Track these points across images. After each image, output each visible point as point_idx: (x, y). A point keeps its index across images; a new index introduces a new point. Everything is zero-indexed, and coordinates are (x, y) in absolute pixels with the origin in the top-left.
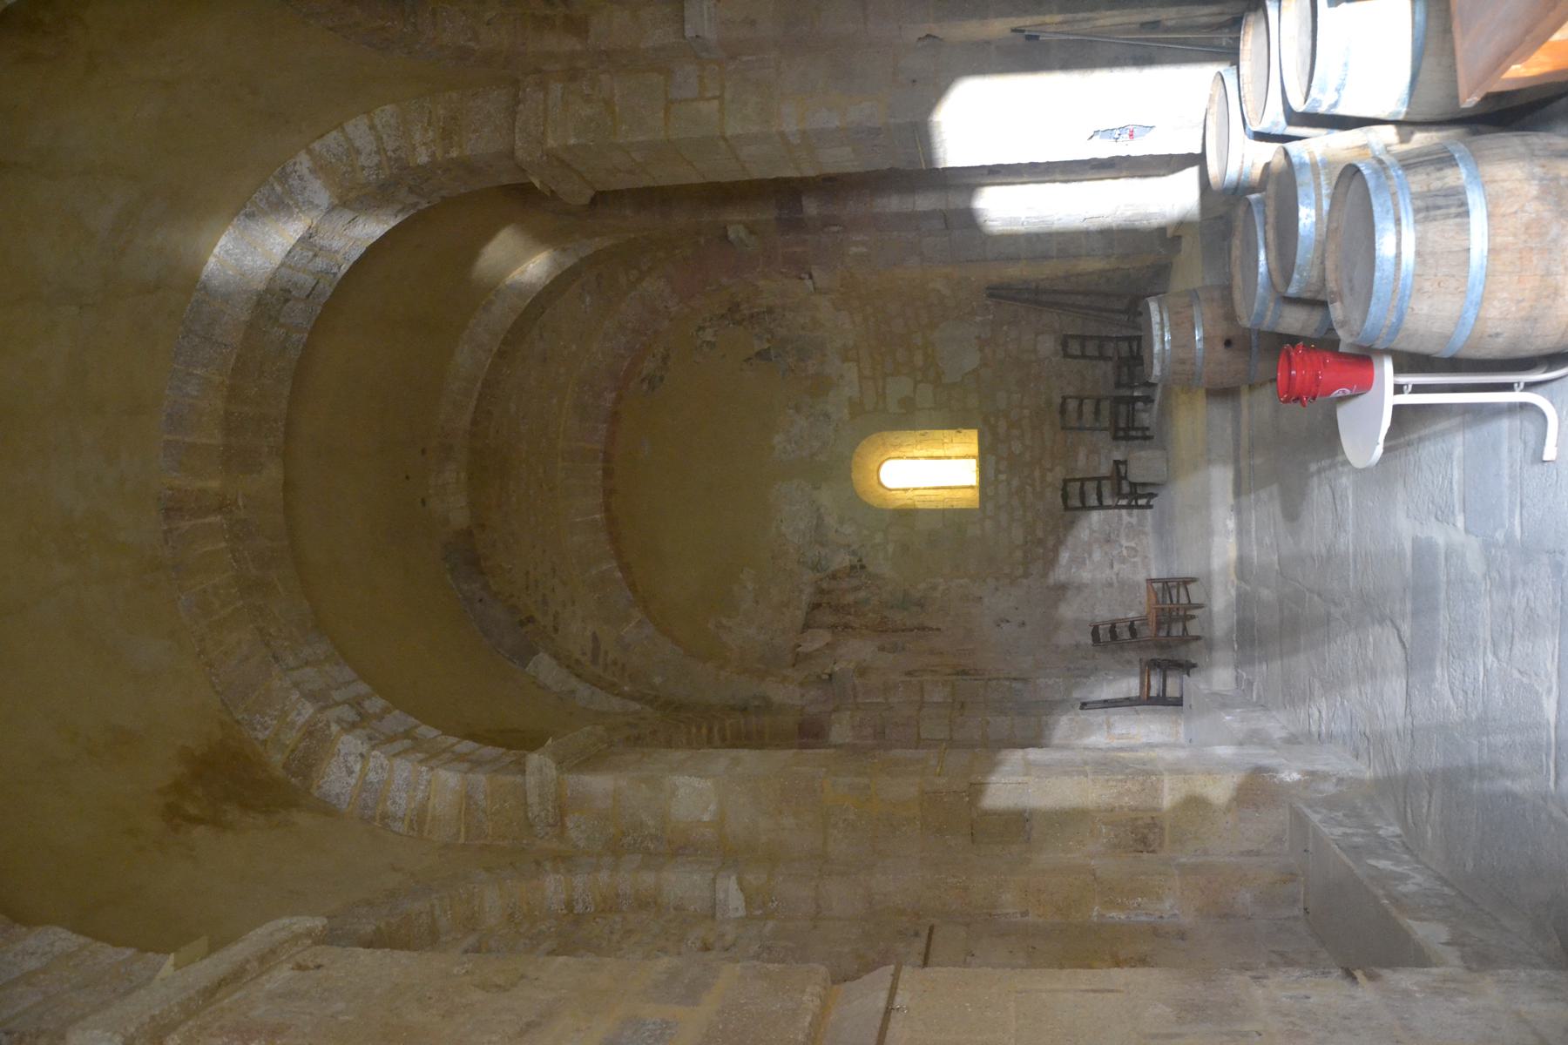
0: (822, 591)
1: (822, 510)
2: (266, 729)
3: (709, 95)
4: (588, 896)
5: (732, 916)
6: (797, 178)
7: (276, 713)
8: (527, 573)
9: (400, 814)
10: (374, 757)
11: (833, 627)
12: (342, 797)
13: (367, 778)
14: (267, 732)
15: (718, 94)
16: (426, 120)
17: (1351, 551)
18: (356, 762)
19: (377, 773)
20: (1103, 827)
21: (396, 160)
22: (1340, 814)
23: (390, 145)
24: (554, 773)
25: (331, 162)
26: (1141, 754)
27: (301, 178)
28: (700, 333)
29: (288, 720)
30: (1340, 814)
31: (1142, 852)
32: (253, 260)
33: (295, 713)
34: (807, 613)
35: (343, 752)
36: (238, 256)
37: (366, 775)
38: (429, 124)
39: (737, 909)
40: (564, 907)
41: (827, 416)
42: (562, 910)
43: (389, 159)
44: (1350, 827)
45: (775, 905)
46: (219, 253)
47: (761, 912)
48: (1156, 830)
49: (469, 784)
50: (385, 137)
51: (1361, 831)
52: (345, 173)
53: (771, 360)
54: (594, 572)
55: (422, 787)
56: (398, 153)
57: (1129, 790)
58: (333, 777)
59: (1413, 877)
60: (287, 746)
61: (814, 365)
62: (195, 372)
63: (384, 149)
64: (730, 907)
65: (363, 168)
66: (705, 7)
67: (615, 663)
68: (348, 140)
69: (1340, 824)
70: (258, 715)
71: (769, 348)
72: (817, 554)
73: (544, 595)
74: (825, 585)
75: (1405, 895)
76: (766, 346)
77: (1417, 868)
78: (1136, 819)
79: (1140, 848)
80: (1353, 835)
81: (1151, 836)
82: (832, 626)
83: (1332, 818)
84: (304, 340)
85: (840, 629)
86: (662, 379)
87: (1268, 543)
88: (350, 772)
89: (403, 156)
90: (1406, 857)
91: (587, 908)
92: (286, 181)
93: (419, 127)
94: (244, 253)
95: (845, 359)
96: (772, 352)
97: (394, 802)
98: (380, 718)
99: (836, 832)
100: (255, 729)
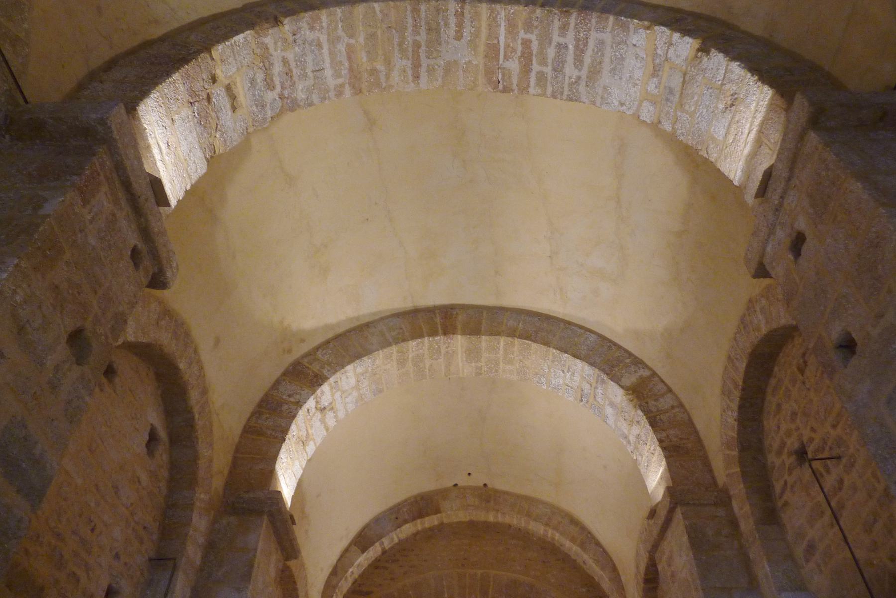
7: (330, 360)
12: (276, 392)
23: (664, 417)
27: (635, 372)
38: (681, 439)
50: (667, 415)
56: (659, 421)
58: (289, 387)
60: (311, 365)
62: (520, 324)
65: (647, 403)
73: (398, 560)
88: (290, 396)
97: (267, 418)
98: (322, 421)
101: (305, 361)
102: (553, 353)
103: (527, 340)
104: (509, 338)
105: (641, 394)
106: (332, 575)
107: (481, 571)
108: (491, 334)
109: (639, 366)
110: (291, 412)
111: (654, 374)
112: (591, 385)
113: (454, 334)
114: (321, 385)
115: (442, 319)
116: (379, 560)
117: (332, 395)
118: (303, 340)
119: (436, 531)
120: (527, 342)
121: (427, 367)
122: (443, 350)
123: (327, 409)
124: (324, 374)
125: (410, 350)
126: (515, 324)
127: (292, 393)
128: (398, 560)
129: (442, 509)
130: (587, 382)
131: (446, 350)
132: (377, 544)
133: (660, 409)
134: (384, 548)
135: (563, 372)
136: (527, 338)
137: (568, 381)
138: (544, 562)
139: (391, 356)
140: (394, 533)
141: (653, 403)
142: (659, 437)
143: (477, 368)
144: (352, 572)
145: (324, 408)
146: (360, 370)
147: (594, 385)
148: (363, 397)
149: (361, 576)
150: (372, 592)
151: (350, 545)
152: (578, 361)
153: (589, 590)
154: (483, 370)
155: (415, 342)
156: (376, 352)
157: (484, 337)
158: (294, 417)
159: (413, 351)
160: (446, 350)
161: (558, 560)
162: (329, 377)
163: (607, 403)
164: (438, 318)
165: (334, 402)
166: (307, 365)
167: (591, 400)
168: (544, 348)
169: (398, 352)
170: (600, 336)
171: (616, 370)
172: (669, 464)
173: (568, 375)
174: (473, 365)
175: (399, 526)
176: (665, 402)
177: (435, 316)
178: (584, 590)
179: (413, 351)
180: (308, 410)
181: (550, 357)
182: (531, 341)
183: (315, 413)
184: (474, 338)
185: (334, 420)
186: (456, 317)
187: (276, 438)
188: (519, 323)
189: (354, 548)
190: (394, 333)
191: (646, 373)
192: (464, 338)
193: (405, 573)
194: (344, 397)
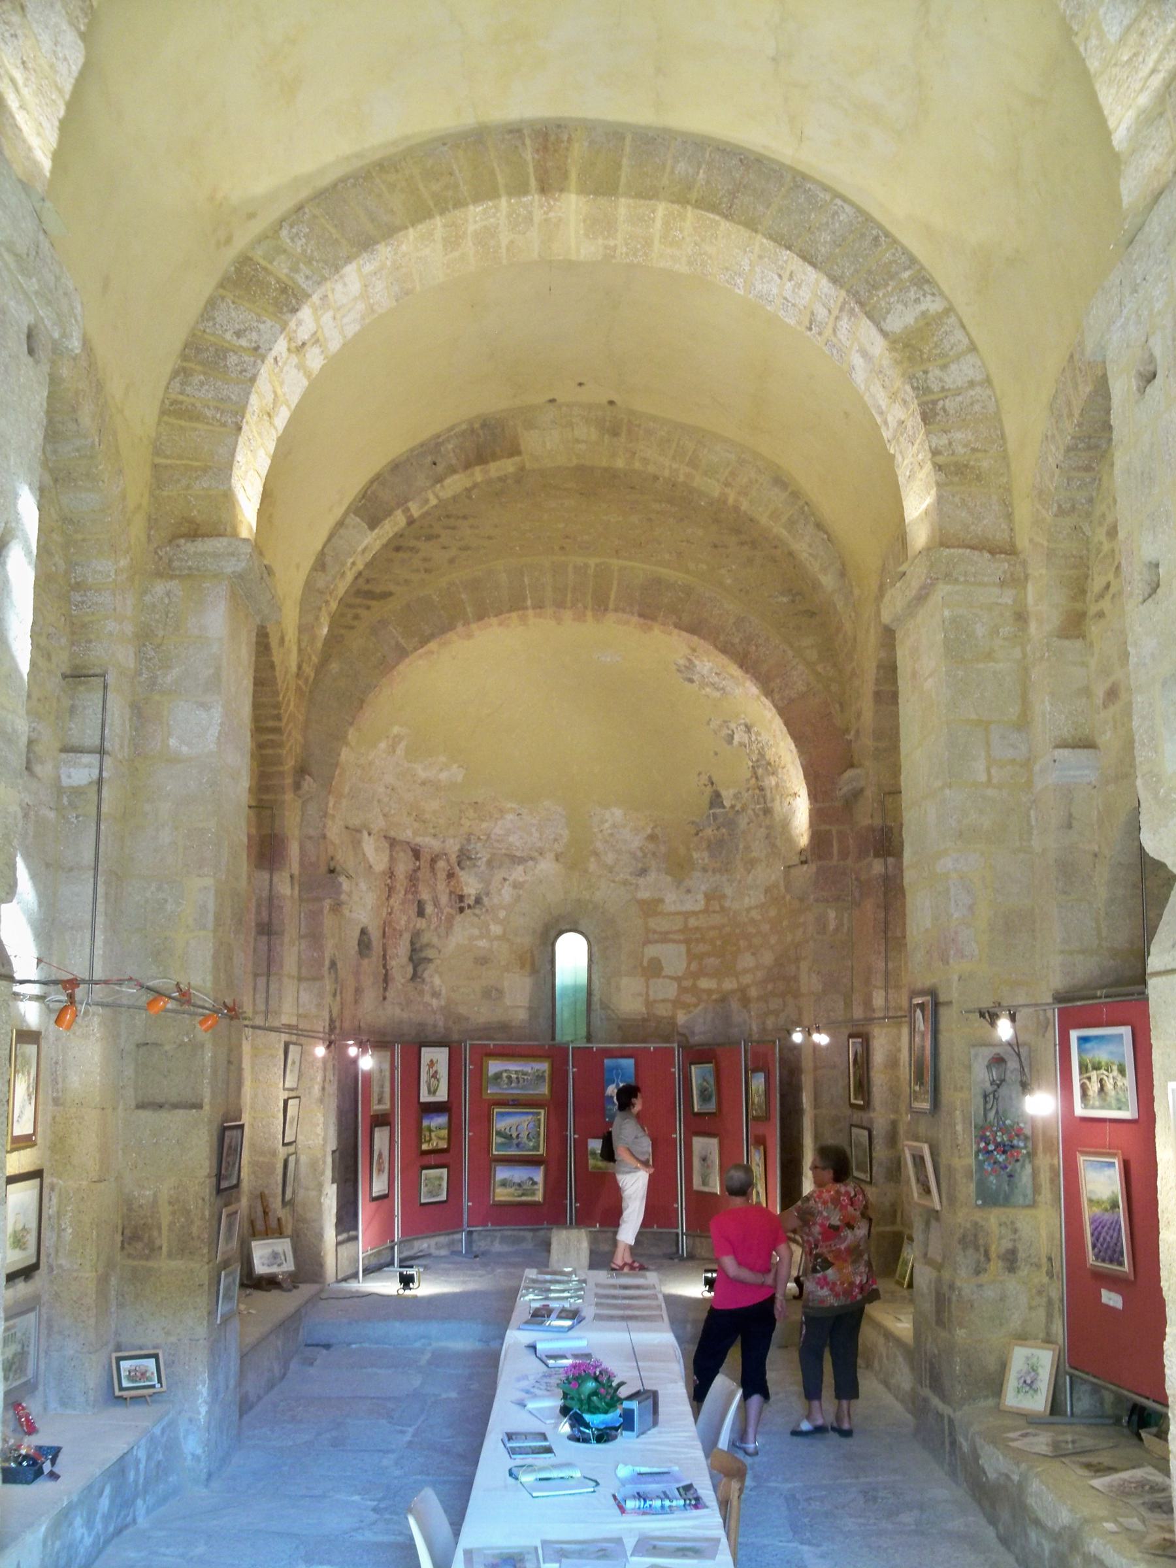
0: (433, 861)
1: (531, 863)
2: (292, 240)
3: (993, 771)
4: (90, 607)
5: (62, 771)
6: (902, 863)
7: (309, 251)
8: (465, 517)
9: (188, 389)
10: (255, 362)
11: (391, 874)
12: (211, 324)
13: (231, 354)
14: (288, 241)
15: (995, 781)
16: (978, 445)
17: (452, 1478)
18: (250, 341)
19: (236, 365)
20: (151, 1192)
21: (932, 410)
22: (160, 1457)
23: (951, 405)
24: (229, 570)
25: (933, 335)
26: (498, 1228)
27: (917, 301)
28: (743, 727)
29: (301, 265)
30: (160, 1457)
31: (123, 1234)
32: (825, 242)
33: (308, 272)
34: (408, 843)
35: (261, 326)
36: (831, 226)
37: (236, 353)
38: (974, 450)
39: (69, 777)
40: (78, 580)
41: (643, 872)
42: (75, 578)
43: (934, 402)
44: (146, 1467)
45: (73, 820)
46: (836, 205)
47: (66, 803)
48: (147, 1252)
49: (220, 470)
50: (959, 399)
51: (141, 1481)
52: (921, 351)
53: (710, 808)
54: (463, 596)
55: (218, 416)
56: (942, 413)
57: (192, 1222)
58: (233, 314)
59: (89, 1535)
60: (271, 262)
61: (703, 859)
62: (701, 171)
63: (946, 397)
64: (72, 770)
65: (926, 372)
66: (1087, 772)
67: (356, 617)
68: (958, 358)
69: (149, 1457)
70: (308, 230)
71: (724, 807)
72: (479, 856)
73: (438, 536)
74: (441, 864)
75: (70, 1525)
76: (727, 803)
77: (99, 1539)
78: (160, 1229)
79: (127, 1232)
80: (137, 1470)
81: (139, 1245)
82: (392, 873)
83: (156, 1448)
84: (737, 291)
85: (389, 881)
86: (691, 681)
87: (472, 1387)
88: (238, 334)
89: (938, 418)
90: (111, 1529)
91: (76, 606)
92: (915, 284)
93: (970, 438)
94: (834, 233)
95: (708, 897)
96: (718, 811)
97: (202, 384)
98: (301, 367)
99: (153, 889)
100: (292, 227)
101: (258, 255)
102: (762, 244)
103: (712, 212)
104: (676, 206)
105: (918, 353)
106: (316, 570)
107: (598, 560)
108: (640, 195)
109: (926, 287)
110: (245, 371)
111: (949, 310)
112: (830, 311)
113: (562, 190)
114: (297, 310)
115: (538, 151)
116: (401, 536)
117: (317, 320)
118: (251, 216)
119: (509, 481)
120: (712, 216)
121: (503, 245)
122: (538, 215)
123: (308, 345)
124: (300, 286)
125: (471, 220)
126: (691, 171)
127: (242, 327)
128: (438, 536)
129: (523, 448)
130: (823, 305)
131: (545, 216)
132: (399, 513)
133: (947, 387)
134: (411, 516)
135: (780, 276)
136: (713, 208)
137: (788, 294)
138: (715, 546)
139: (432, 235)
140: (430, 492)
141: (937, 372)
142: (934, 445)
143: (606, 247)
144: (354, 564)
145: (304, 344)
146: (369, 268)
147: (835, 312)
148: (375, 307)
149: (369, 565)
150: (390, 594)
151: (346, 514)
152: (810, 269)
153: (793, 601)
154: (618, 252)
155: (481, 208)
156: (402, 233)
157: (623, 200)
158: (253, 379)
159: (475, 222)
160: (545, 216)
161: (742, 544)
162: (310, 292)
163: (856, 347)
164: (529, 150)
165: (320, 330)
166: (264, 263)
167: (828, 332)
168: (745, 233)
169: (445, 226)
170: (859, 210)
171: (881, 295)
172: (940, 499)
173: (789, 285)
174: (600, 241)
175: (439, 480)
176: (959, 373)
177: (524, 144)
178: (785, 600)
179: (475, 222)
180: (276, 359)
181: (757, 248)
182: (719, 214)
183: (288, 359)
184: (603, 201)
185: (322, 357)
186: (567, 149)
187: (224, 425)
188: (699, 167)
189: (354, 520)
190: (436, 187)
191: (933, 306)
192: (583, 199)
193: (452, 561)
194: (338, 316)
